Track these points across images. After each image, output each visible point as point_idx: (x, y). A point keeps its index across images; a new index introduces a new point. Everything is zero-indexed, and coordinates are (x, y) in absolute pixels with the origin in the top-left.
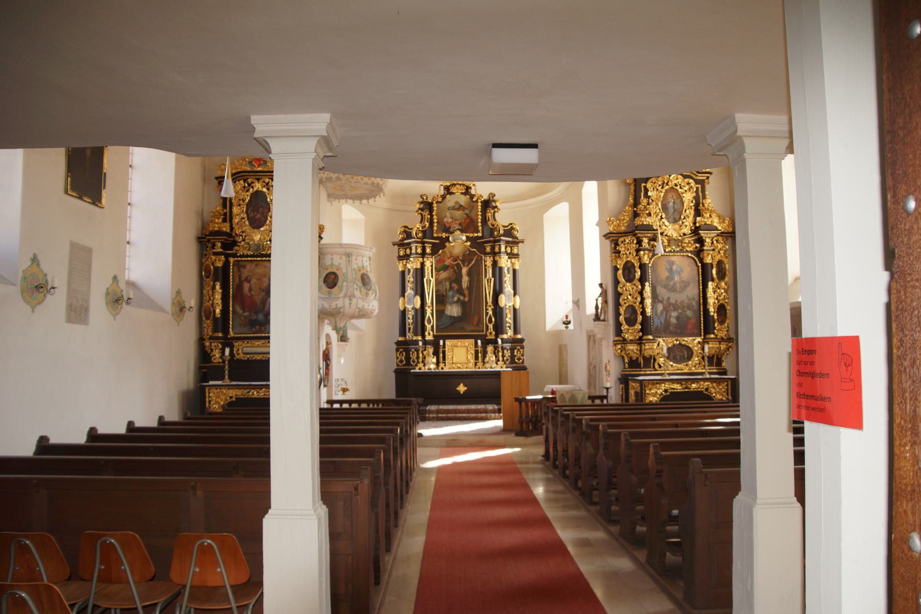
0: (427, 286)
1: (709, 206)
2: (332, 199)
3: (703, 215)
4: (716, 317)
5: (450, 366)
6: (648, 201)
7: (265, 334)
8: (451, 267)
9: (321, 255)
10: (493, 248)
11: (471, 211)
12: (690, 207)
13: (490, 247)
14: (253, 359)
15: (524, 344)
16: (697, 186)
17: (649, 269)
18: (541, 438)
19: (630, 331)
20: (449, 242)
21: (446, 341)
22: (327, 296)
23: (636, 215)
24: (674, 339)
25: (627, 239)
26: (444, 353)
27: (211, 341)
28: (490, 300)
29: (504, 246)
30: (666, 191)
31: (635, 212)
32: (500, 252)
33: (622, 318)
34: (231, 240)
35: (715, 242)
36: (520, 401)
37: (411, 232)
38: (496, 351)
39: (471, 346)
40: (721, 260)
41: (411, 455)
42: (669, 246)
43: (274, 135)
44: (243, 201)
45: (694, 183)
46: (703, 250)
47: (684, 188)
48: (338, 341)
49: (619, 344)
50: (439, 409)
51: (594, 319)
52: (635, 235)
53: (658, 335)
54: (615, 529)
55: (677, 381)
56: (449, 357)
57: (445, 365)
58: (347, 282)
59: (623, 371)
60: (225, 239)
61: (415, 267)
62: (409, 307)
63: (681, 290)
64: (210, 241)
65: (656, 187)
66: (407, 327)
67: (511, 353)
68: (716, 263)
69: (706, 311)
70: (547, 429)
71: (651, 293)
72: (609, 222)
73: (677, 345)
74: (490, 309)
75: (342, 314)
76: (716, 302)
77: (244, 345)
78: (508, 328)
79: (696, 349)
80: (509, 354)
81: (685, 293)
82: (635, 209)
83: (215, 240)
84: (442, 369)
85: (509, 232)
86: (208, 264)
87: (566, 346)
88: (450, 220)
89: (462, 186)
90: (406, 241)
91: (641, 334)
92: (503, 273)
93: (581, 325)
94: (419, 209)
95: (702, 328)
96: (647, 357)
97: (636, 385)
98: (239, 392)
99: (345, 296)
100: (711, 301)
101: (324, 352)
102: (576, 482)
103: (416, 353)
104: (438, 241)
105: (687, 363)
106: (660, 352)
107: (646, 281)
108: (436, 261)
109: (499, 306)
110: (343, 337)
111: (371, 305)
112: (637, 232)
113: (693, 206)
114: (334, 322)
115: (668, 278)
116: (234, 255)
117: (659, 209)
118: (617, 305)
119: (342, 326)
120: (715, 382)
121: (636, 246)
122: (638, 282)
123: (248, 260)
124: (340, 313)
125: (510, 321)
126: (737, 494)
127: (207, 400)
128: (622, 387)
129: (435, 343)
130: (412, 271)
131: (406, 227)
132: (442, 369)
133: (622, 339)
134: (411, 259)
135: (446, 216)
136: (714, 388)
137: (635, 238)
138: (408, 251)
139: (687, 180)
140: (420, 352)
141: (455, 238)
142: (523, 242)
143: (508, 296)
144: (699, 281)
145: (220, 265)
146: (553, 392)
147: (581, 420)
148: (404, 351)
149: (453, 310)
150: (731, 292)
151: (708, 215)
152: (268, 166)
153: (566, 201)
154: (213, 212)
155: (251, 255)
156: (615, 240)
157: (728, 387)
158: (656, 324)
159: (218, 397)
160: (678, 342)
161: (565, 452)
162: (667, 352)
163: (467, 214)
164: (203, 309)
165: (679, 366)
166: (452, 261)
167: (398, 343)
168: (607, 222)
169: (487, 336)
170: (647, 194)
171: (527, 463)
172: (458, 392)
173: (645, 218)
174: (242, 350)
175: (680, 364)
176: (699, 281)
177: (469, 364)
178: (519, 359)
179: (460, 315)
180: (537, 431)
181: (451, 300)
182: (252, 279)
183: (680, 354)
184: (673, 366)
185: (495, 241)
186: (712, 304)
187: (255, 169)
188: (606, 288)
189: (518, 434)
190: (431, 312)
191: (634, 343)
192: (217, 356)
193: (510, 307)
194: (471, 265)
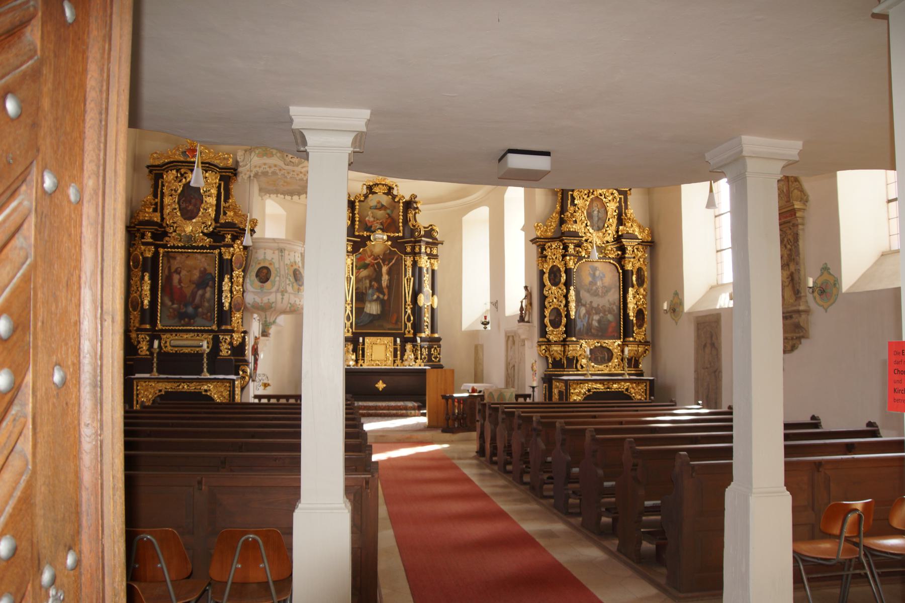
2: (263, 194)
3: (625, 224)
4: (635, 322)
7: (194, 327)
8: (372, 266)
10: (413, 248)
11: (392, 211)
14: (181, 352)
15: (441, 343)
16: (620, 196)
20: (370, 240)
21: (366, 338)
22: (259, 291)
23: (562, 222)
24: (595, 342)
25: (554, 244)
26: (363, 350)
27: (138, 333)
28: (409, 299)
30: (592, 199)
32: (420, 253)
33: (547, 320)
34: (162, 231)
35: (635, 250)
36: (447, 398)
38: (414, 349)
39: (390, 344)
40: (641, 268)
44: (176, 191)
47: (608, 197)
51: (518, 321)
52: (561, 241)
53: (581, 337)
55: (600, 382)
57: (364, 362)
58: (280, 277)
59: (546, 371)
60: (157, 230)
63: (603, 295)
64: (140, 231)
65: (582, 196)
67: (428, 351)
68: (636, 270)
69: (626, 315)
70: (482, 427)
72: (537, 228)
73: (598, 347)
74: (408, 307)
75: (272, 309)
76: (636, 307)
77: (171, 338)
78: (426, 327)
79: (616, 351)
80: (427, 353)
82: (562, 216)
83: (145, 230)
84: (361, 365)
85: (429, 233)
86: (136, 254)
87: (482, 346)
88: (372, 219)
89: (384, 186)
91: (565, 335)
95: (622, 331)
96: (570, 358)
97: (561, 386)
100: (631, 306)
101: (253, 347)
102: (521, 477)
104: (359, 240)
105: (607, 364)
106: (582, 354)
107: (570, 286)
108: (356, 259)
110: (265, 332)
115: (591, 283)
116: (165, 246)
118: (542, 307)
119: (272, 321)
120: (635, 383)
121: (562, 252)
122: (563, 285)
123: (178, 252)
124: (272, 308)
125: (428, 320)
126: (729, 484)
127: (135, 392)
128: (545, 386)
132: (361, 365)
133: (546, 340)
136: (633, 388)
137: (561, 244)
142: (442, 244)
144: (620, 287)
145: (149, 256)
147: (532, 417)
149: (373, 308)
150: (648, 298)
151: (630, 224)
153: (486, 205)
154: (144, 201)
156: (542, 245)
159: (146, 390)
160: (599, 344)
163: (388, 214)
164: (130, 300)
165: (600, 367)
166: (373, 259)
168: (535, 227)
169: (405, 334)
170: (574, 202)
172: (377, 389)
173: (572, 225)
174: (170, 343)
175: (601, 365)
176: (620, 287)
177: (387, 361)
178: (436, 358)
179: (379, 312)
182: (182, 271)
183: (601, 356)
185: (416, 242)
186: (631, 308)
187: (189, 159)
190: (351, 309)
191: (558, 344)
192: (144, 348)
193: (428, 306)
194: (391, 264)
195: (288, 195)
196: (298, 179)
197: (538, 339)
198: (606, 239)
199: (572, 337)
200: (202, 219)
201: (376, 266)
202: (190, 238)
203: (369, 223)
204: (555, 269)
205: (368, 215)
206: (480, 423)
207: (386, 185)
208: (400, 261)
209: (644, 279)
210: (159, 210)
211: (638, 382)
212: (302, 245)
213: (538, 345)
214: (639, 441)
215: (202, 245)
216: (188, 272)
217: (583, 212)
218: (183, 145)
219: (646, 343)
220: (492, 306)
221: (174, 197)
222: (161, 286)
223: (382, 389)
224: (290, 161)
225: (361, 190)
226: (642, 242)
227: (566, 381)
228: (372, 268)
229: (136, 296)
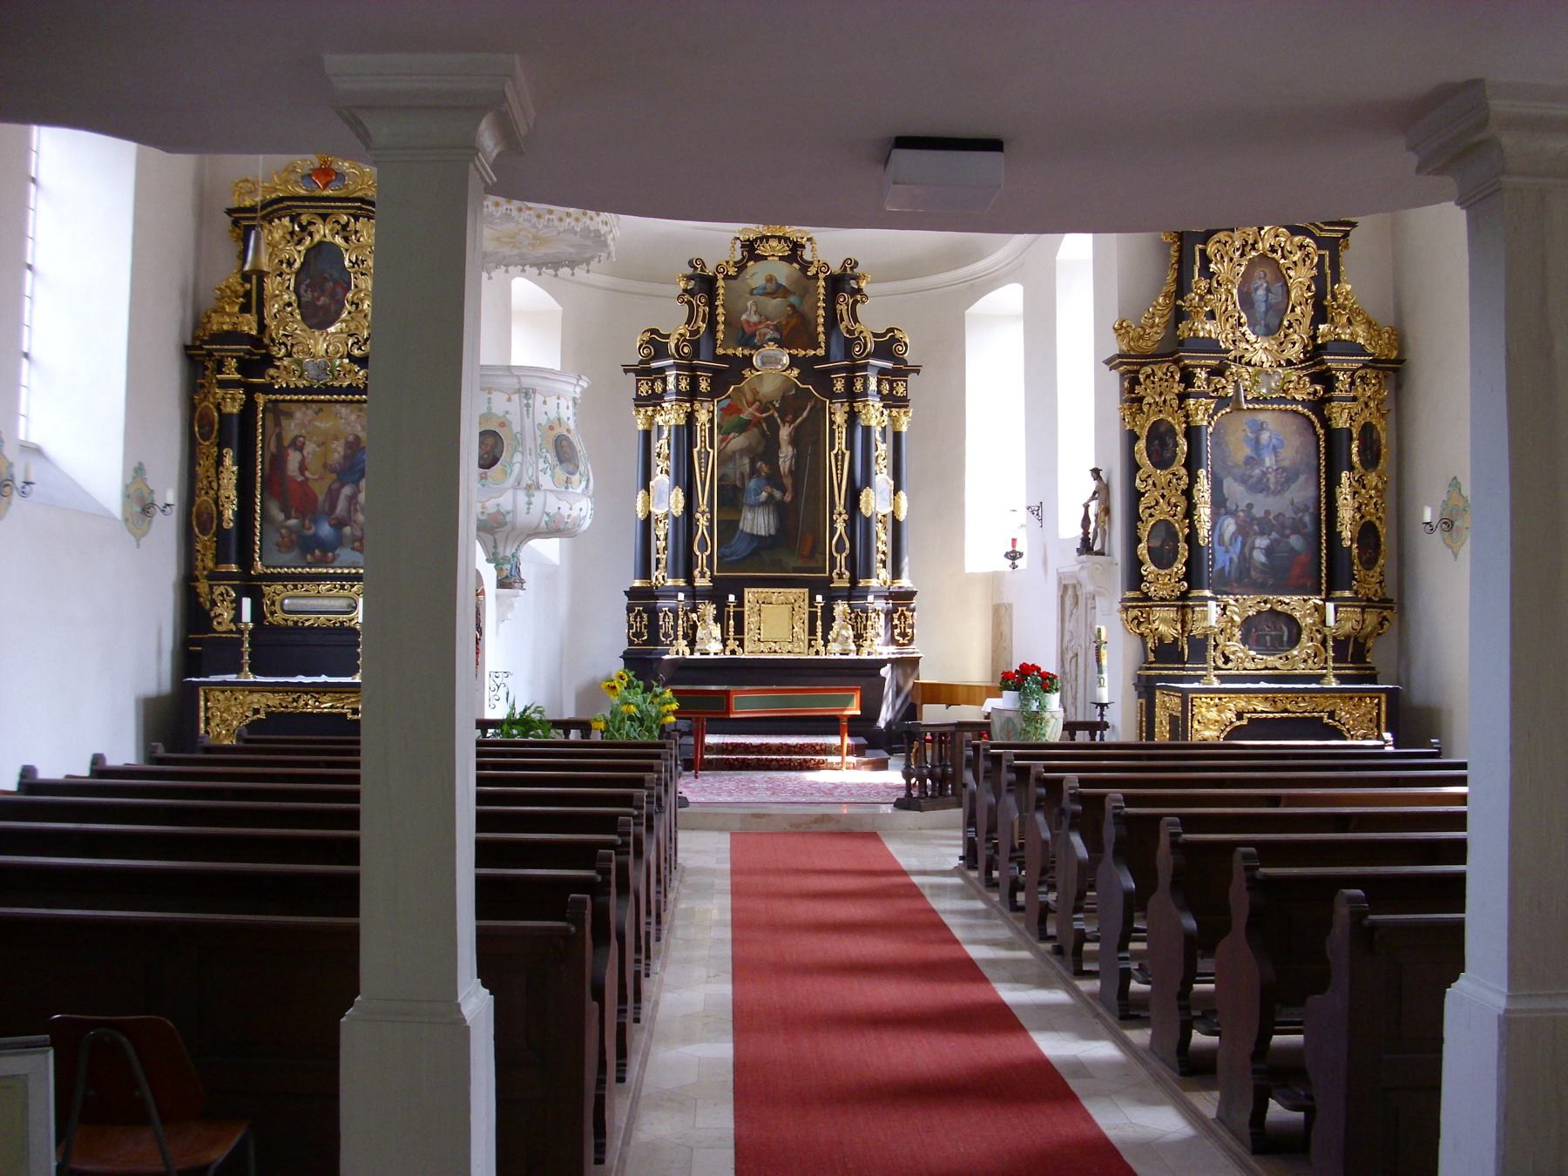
3: (1332, 319)
8: (755, 426)
10: (850, 383)
15: (915, 603)
16: (1322, 252)
18: (957, 815)
20: (752, 366)
23: (1179, 315)
32: (865, 393)
33: (1142, 549)
40: (1370, 423)
44: (290, 264)
45: (1315, 246)
52: (1176, 362)
60: (248, 352)
65: (1227, 252)
66: (654, 556)
69: (1334, 536)
81: (1288, 495)
85: (887, 346)
87: (1009, 607)
91: (1186, 584)
94: (685, 291)
97: (1174, 702)
100: (1346, 514)
108: (721, 409)
111: (576, 507)
113: (1311, 297)
115: (1251, 461)
116: (267, 389)
118: (1133, 518)
119: (508, 553)
123: (298, 401)
126: (1456, 979)
129: (716, 595)
134: (663, 405)
139: (1297, 239)
142: (918, 372)
149: (758, 522)
151: (1344, 320)
154: (220, 289)
160: (1269, 606)
164: (194, 509)
167: (633, 594)
179: (772, 532)
182: (307, 442)
187: (318, 193)
190: (708, 524)
197: (1123, 594)
198: (1286, 355)
199: (1201, 588)
201: (764, 425)
202: (326, 368)
204: (1162, 428)
205: (746, 310)
207: (787, 239)
210: (254, 310)
213: (1123, 606)
214: (1271, 853)
215: (350, 385)
216: (318, 446)
217: (1229, 291)
221: (288, 277)
226: (1375, 361)
227: (1184, 692)
229: (207, 501)
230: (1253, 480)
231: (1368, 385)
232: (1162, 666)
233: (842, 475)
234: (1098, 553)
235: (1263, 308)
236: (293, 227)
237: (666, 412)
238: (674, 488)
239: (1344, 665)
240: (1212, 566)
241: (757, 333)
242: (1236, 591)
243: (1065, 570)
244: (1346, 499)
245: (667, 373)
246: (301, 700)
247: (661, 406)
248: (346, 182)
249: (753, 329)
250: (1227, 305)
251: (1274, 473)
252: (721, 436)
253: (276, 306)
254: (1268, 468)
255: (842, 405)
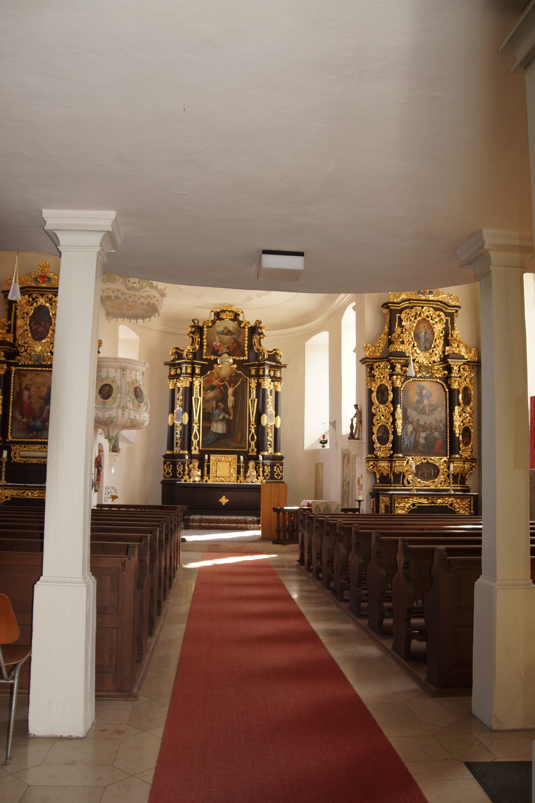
0: (195, 404)
1: (457, 337)
2: (111, 318)
3: (451, 345)
4: (461, 439)
5: (214, 479)
6: (402, 330)
8: (218, 388)
9: (100, 365)
10: (258, 371)
11: (238, 336)
12: (440, 338)
13: (255, 370)
14: (29, 462)
15: (283, 461)
16: (447, 318)
17: (401, 393)
18: (296, 546)
19: (382, 449)
20: (217, 364)
21: (211, 455)
22: (102, 406)
23: (390, 342)
26: (208, 467)
28: (253, 419)
29: (268, 369)
31: (389, 339)
32: (264, 375)
33: (374, 437)
35: (462, 370)
36: (278, 511)
37: (182, 353)
38: (257, 467)
39: (234, 461)
40: (467, 387)
41: (174, 553)
42: (420, 372)
43: (63, 228)
44: (27, 314)
45: (444, 315)
46: (451, 377)
48: (110, 451)
49: (371, 461)
50: (202, 519)
51: (348, 438)
52: (389, 361)
54: (364, 622)
56: (213, 471)
57: (209, 478)
59: (374, 486)
60: (9, 349)
61: (184, 386)
62: (178, 423)
65: (409, 317)
66: (175, 441)
67: (270, 469)
69: (452, 433)
70: (303, 536)
71: (403, 415)
72: (366, 348)
74: (252, 427)
75: (114, 424)
80: (270, 471)
81: (434, 416)
82: (390, 337)
84: (206, 481)
85: (273, 356)
87: (322, 464)
88: (219, 344)
89: (231, 312)
90: (176, 362)
91: (392, 452)
92: (266, 395)
93: (336, 445)
94: (191, 332)
95: (448, 448)
98: (14, 493)
99: (118, 407)
100: (457, 424)
101: (96, 459)
102: (328, 582)
103: (182, 466)
104: (207, 363)
108: (204, 381)
109: (261, 424)
110: (115, 448)
111: (142, 416)
112: (390, 358)
113: (443, 336)
114: (107, 431)
115: (418, 402)
116: (16, 365)
117: (412, 338)
118: (371, 424)
119: (114, 435)
120: (459, 498)
121: (389, 371)
122: (390, 403)
123: (29, 370)
124: (113, 422)
125: (271, 439)
128: (373, 501)
129: (200, 458)
130: (181, 389)
131: (177, 348)
132: (206, 481)
134: (181, 378)
135: (215, 340)
136: (458, 503)
138: (179, 371)
139: (437, 313)
140: (186, 465)
141: (223, 361)
142: (285, 367)
143: (270, 416)
145: (2, 373)
146: (309, 505)
148: (171, 464)
149: (219, 428)
150: (475, 416)
151: (456, 345)
152: (52, 283)
155: (32, 364)
157: (470, 503)
158: (405, 444)
160: (426, 461)
161: (319, 556)
162: (415, 469)
163: (234, 339)
167: (166, 456)
168: (364, 348)
170: (402, 324)
171: (283, 567)
172: (221, 503)
173: (399, 345)
174: (19, 454)
175: (428, 481)
178: (278, 475)
179: (225, 432)
180: (293, 540)
181: (217, 417)
182: (32, 387)
184: (421, 484)
187: (40, 285)
188: (361, 410)
189: (275, 542)
190: (198, 428)
193: (271, 426)
195: (133, 319)
196: (139, 303)
197: (367, 455)
198: (433, 359)
200: (50, 340)
203: (217, 347)
204: (383, 388)
206: (301, 532)
207: (232, 312)
208: (245, 384)
209: (470, 398)
210: (12, 332)
211: (462, 498)
212: (143, 365)
213: (366, 461)
216: (37, 388)
218: (35, 272)
219: (473, 460)
220: (331, 425)
221: (26, 319)
222: (13, 401)
223: (220, 502)
224: (132, 286)
225: (209, 317)
228: (218, 390)
230: (419, 410)
231: (466, 371)
232: (382, 485)
233: (254, 408)
234: (357, 439)
235: (423, 340)
236: (29, 299)
237: (181, 382)
238: (184, 412)
239: (456, 485)
240: (403, 444)
241: (220, 350)
242: (412, 455)
243: (344, 448)
244: (457, 417)
245: (182, 365)
246: (26, 493)
247: (179, 379)
248: (52, 281)
249: (218, 348)
250: (409, 339)
251: (428, 407)
252: (204, 392)
253: (21, 331)
254: (425, 405)
255: (254, 380)
